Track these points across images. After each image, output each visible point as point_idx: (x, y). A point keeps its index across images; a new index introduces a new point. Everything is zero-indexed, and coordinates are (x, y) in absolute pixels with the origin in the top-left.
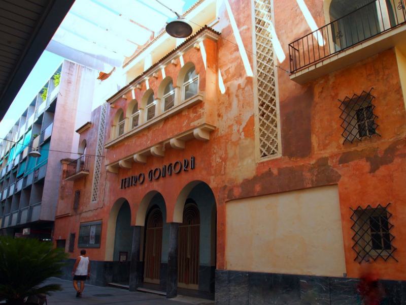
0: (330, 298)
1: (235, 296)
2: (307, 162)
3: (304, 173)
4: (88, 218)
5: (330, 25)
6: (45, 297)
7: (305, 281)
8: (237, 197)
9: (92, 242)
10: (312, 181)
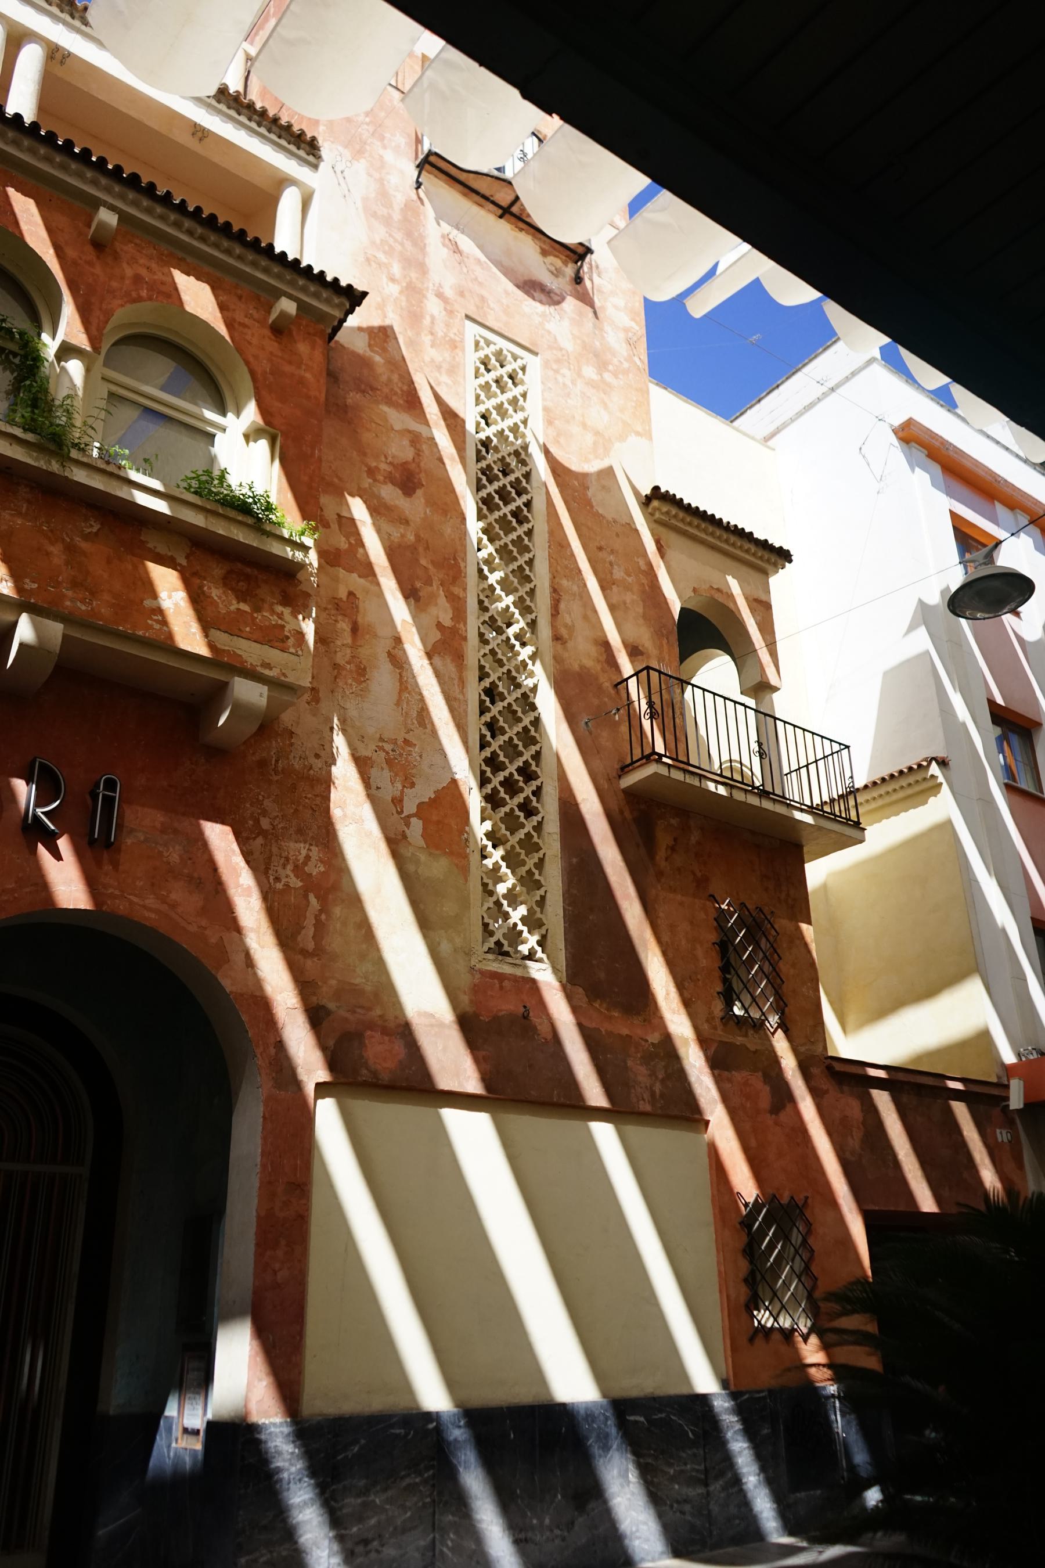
0: (705, 1460)
1: (366, 1542)
2: (639, 1032)
3: (630, 1063)
4: (258, 298)
5: (635, 678)
6: (214, 436)
7: (642, 1419)
8: (385, 1077)
9: (216, 482)
10: (653, 1094)
